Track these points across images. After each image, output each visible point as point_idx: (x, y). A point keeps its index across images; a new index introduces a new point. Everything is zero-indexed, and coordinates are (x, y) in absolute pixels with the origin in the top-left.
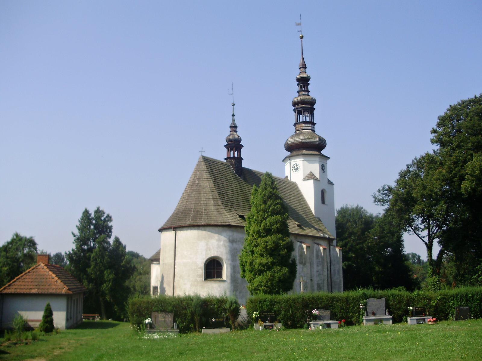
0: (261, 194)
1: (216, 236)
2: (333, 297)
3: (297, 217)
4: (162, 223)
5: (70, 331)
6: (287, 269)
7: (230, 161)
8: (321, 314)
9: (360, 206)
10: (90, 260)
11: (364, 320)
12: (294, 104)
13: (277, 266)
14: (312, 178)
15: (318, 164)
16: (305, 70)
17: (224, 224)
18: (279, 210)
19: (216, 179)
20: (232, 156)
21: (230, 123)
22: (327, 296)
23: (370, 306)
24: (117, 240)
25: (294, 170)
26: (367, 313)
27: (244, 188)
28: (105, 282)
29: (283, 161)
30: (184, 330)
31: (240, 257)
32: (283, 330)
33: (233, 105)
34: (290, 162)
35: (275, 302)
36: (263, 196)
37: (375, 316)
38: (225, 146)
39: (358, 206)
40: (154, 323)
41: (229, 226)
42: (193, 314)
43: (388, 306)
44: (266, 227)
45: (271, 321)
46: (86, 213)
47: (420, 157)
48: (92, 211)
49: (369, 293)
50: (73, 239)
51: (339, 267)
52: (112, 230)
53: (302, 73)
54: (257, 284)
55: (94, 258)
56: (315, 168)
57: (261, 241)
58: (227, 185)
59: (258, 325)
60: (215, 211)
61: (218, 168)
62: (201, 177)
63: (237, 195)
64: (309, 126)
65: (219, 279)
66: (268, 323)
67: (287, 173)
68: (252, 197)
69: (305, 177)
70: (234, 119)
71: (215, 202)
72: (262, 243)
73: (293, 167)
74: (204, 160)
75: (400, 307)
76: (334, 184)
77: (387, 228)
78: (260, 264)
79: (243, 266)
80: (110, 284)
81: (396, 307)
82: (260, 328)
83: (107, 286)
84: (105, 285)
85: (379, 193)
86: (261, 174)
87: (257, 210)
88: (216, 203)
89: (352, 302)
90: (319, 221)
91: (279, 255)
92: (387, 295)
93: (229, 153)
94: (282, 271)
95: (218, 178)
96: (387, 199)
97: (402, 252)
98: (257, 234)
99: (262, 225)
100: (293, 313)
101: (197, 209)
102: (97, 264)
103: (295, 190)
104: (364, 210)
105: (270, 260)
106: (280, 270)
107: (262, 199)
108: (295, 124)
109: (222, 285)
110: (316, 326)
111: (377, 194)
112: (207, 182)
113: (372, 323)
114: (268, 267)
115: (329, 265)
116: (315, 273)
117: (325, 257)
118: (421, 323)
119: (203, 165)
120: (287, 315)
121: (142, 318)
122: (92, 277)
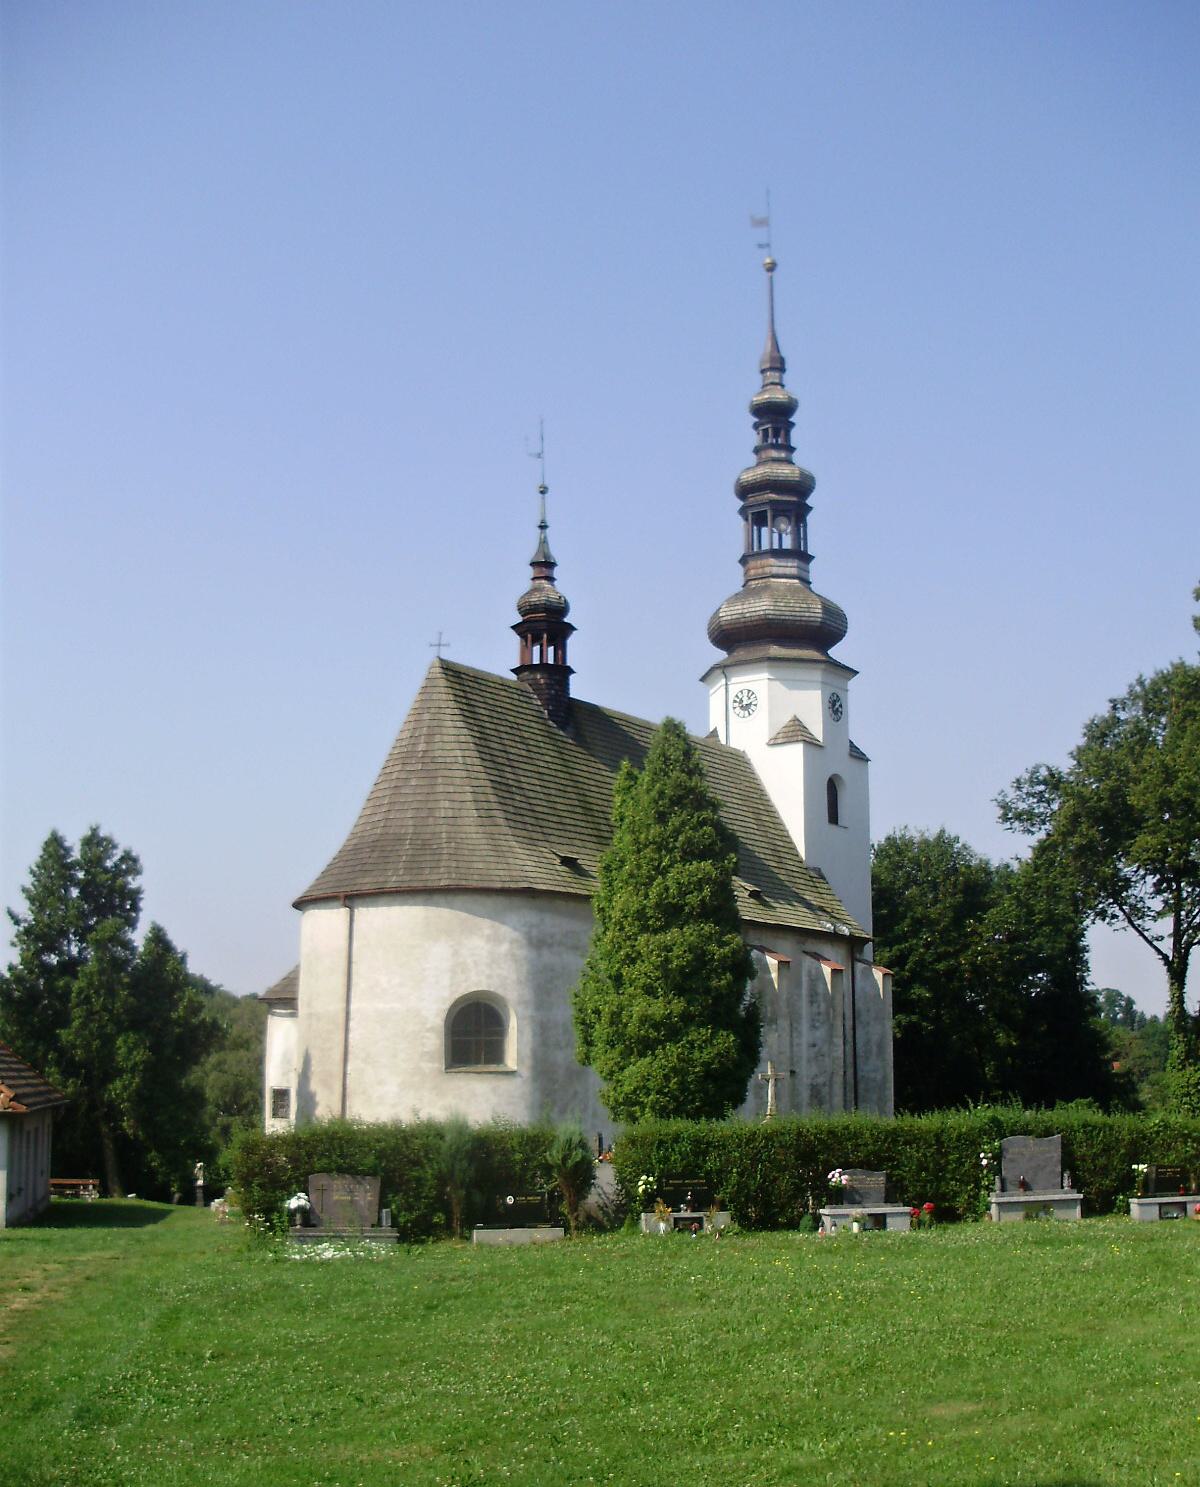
0: (648, 791)
1: (486, 926)
2: (895, 1129)
3: (753, 869)
4: (303, 882)
5: (20, 1232)
6: (732, 1038)
7: (532, 676)
8: (856, 1185)
9: (951, 832)
10: (68, 1000)
11: (993, 1206)
12: (744, 491)
13: (699, 1027)
14: (800, 738)
15: (820, 692)
16: (781, 378)
17: (513, 885)
18: (710, 845)
19: (486, 736)
20: (536, 661)
21: (530, 552)
22: (875, 1126)
23: (1012, 1161)
24: (158, 938)
25: (738, 710)
26: (1003, 1181)
27: (577, 766)
28: (120, 1072)
29: (703, 679)
30: (412, 1233)
31: (576, 996)
32: (736, 1234)
33: (544, 491)
34: (726, 684)
35: (709, 1144)
36: (657, 798)
37: (1027, 1193)
38: (513, 627)
39: (943, 831)
40: (317, 1210)
41: (530, 893)
42: (442, 1180)
43: (1069, 1162)
44: (666, 898)
45: (696, 1205)
46: (55, 846)
47: (1152, 675)
48: (74, 841)
49: (1011, 1119)
50: (11, 931)
51: (882, 1030)
52: (142, 904)
53: (772, 387)
54: (635, 1084)
55: (82, 997)
56: (808, 704)
57: (648, 946)
58: (521, 759)
59: (653, 1217)
60: (484, 841)
61: (491, 702)
62: (437, 730)
63: (553, 792)
64: (790, 566)
65: (493, 1068)
66: (685, 1213)
67: (716, 721)
68: (618, 800)
69: (773, 736)
70: (545, 537)
71: (483, 813)
72: (653, 951)
73: (735, 701)
74: (446, 674)
75: (1106, 1166)
76: (868, 760)
77: (1041, 905)
78: (644, 1020)
79: (587, 1026)
80: (137, 1080)
81: (1095, 1166)
82: (662, 1226)
83: (125, 1088)
84: (118, 1084)
85: (1018, 793)
86: (646, 727)
87: (636, 841)
88: (486, 817)
89: (957, 1147)
90: (822, 881)
91: (708, 991)
92: (1067, 1126)
93: (526, 650)
94: (718, 1044)
95: (493, 733)
96: (1042, 813)
97: (1082, 988)
98: (636, 923)
99: (653, 892)
100: (765, 1181)
101: (423, 837)
102: (90, 1013)
103: (742, 778)
104: (964, 847)
105: (678, 1005)
106: (708, 1042)
107: (652, 805)
108: (744, 556)
109: (505, 1085)
110: (839, 1222)
111: (1012, 794)
112: (454, 742)
113: (1017, 1216)
114: (671, 1031)
115: (849, 1023)
116: (804, 1052)
117: (839, 998)
118: (1173, 1218)
119: (443, 690)
120: (747, 1186)
121: (278, 1193)
122: (77, 1059)
